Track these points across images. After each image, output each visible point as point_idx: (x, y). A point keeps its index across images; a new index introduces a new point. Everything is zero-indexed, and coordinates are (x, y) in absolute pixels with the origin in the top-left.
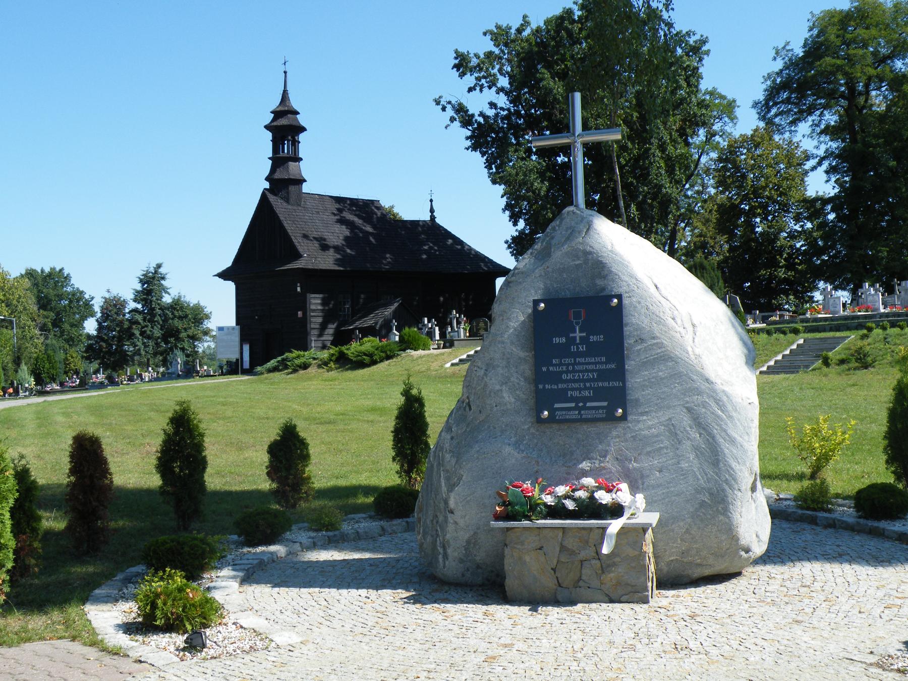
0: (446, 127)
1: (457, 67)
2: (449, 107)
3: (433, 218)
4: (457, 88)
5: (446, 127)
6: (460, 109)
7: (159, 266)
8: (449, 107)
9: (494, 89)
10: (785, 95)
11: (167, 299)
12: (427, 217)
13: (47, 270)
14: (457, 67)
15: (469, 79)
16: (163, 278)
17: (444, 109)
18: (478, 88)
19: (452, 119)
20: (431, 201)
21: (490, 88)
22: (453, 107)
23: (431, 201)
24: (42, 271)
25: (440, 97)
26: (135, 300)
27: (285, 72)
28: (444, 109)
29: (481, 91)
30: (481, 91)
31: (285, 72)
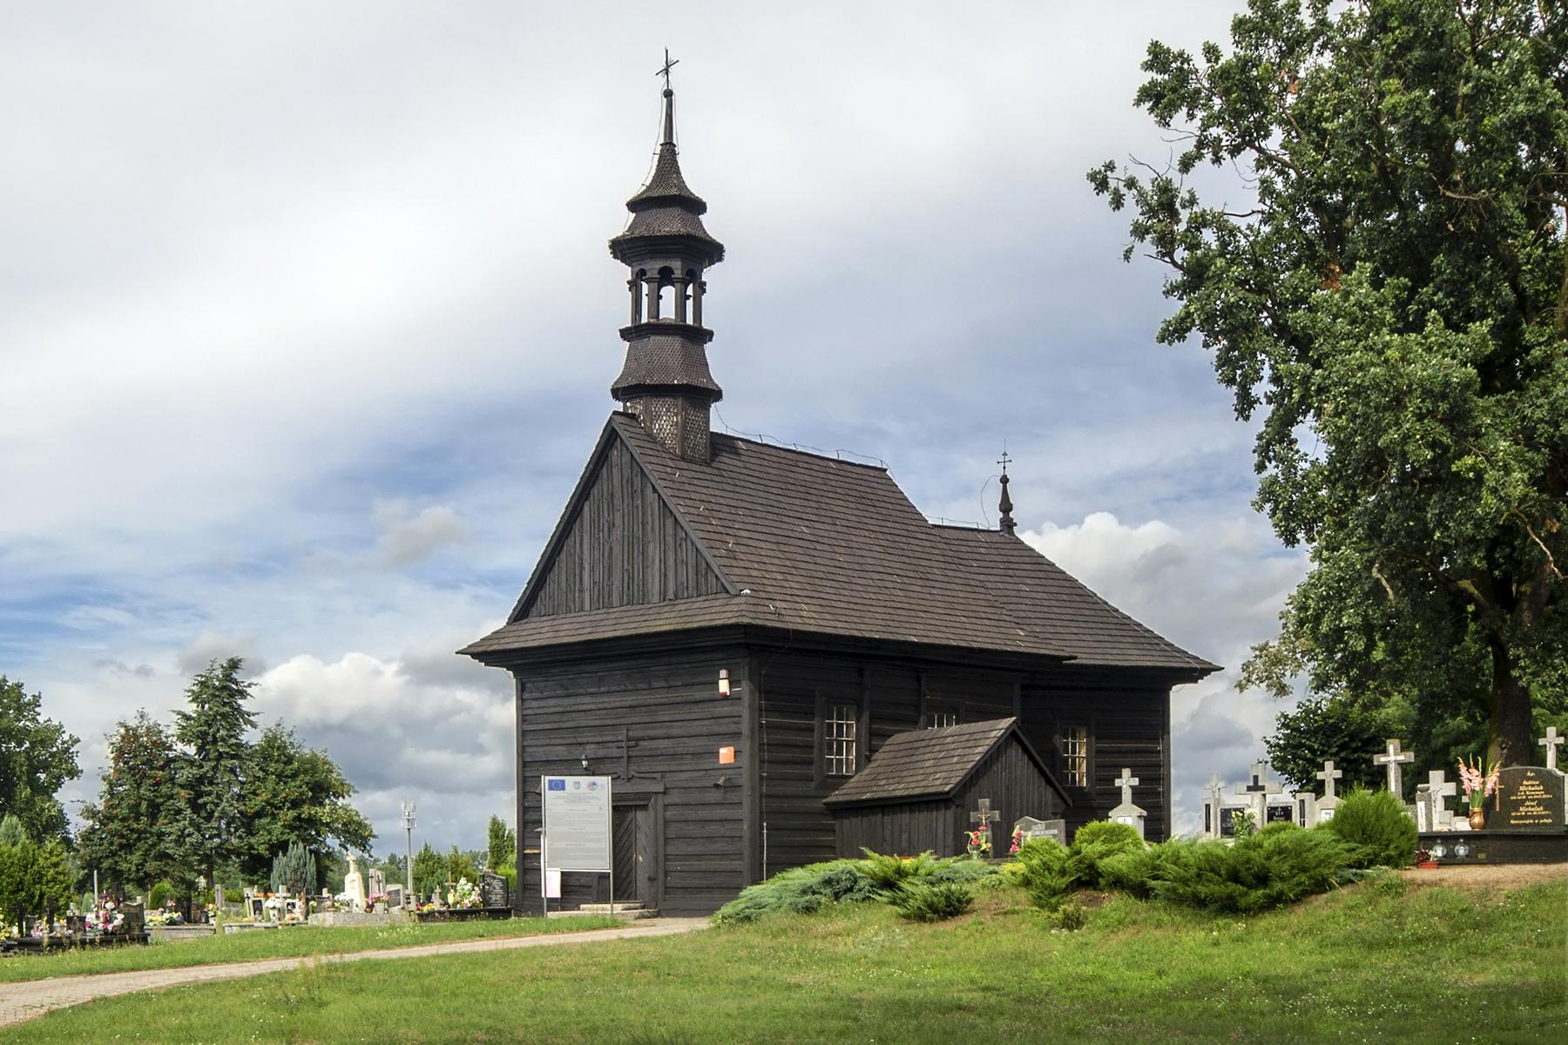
0: (1127, 257)
1: (1149, 94)
2: (1130, 197)
3: (1008, 524)
4: (1154, 147)
5: (1127, 257)
6: (1165, 202)
7: (234, 665)
8: (1130, 197)
11: (251, 737)
12: (993, 522)
15: (1185, 128)
16: (243, 694)
17: (1117, 202)
18: (1208, 155)
19: (1140, 232)
20: (1004, 480)
22: (1142, 198)
23: (1004, 480)
24: (1151, 110)
25: (1110, 167)
27: (668, 94)
28: (1117, 202)
29: (1217, 160)
30: (1217, 160)
31: (668, 94)
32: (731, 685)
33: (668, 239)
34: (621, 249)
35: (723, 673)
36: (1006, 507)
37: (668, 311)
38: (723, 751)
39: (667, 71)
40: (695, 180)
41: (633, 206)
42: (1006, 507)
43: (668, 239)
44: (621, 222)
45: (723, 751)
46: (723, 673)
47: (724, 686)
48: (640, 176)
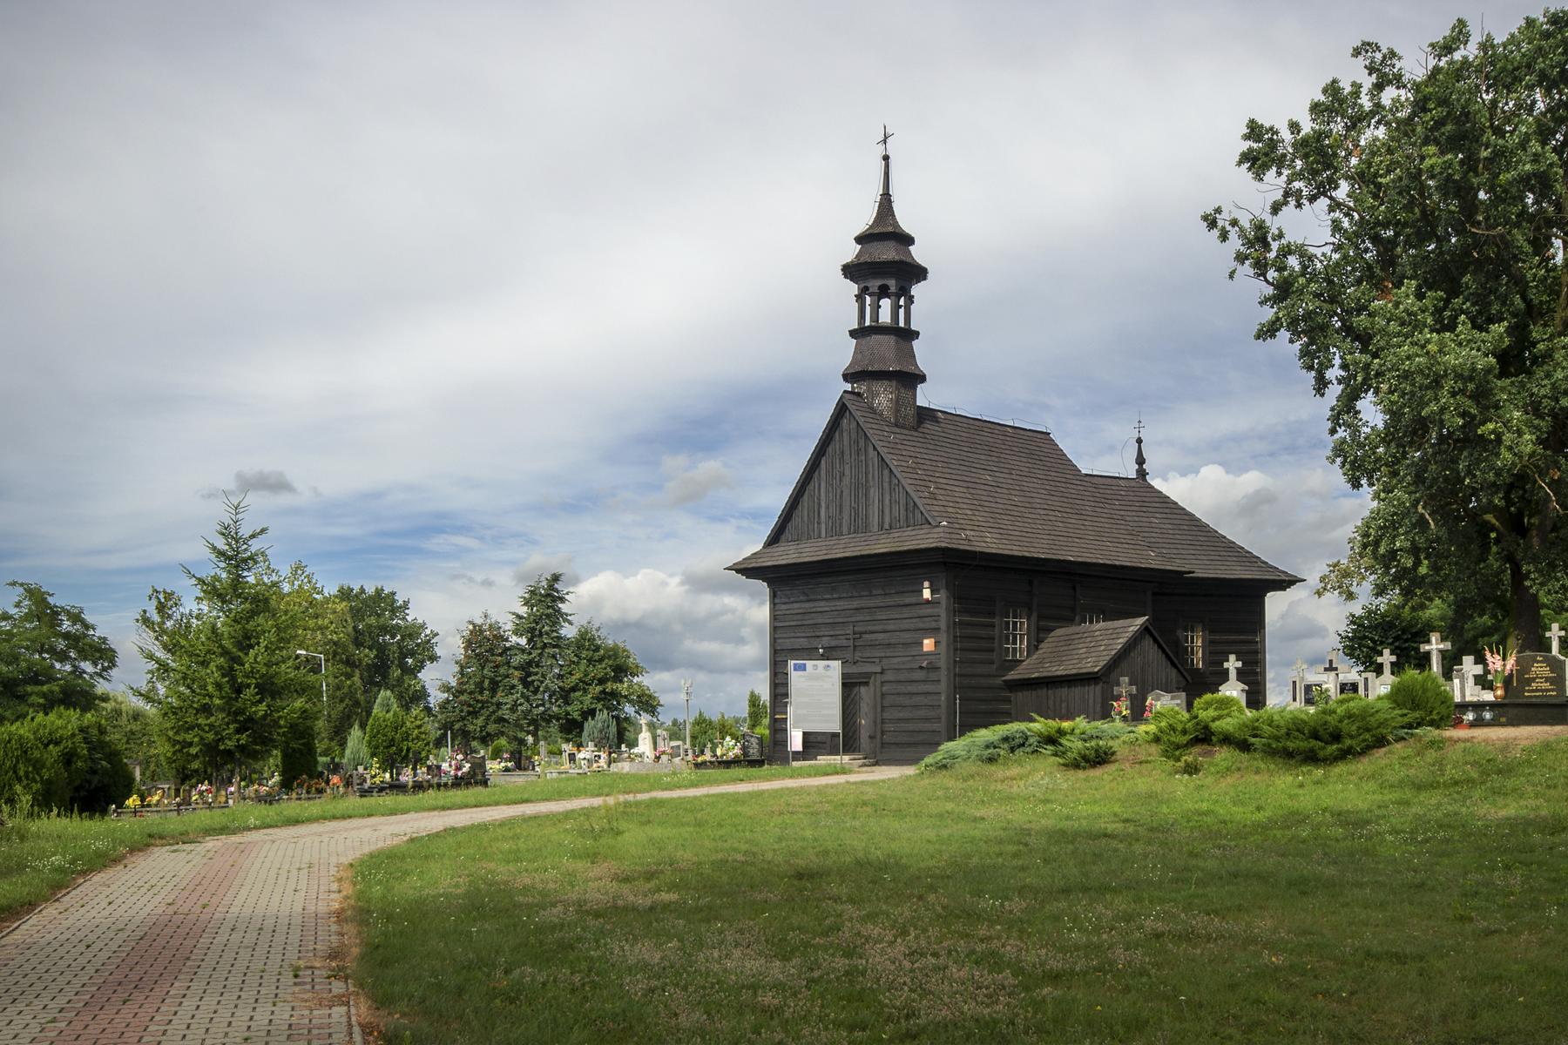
0: (1231, 276)
1: (1248, 158)
2: (1233, 233)
3: (1142, 474)
4: (1252, 197)
7: (556, 578)
8: (1233, 233)
9: (1323, 202)
10: (1359, 379)
11: (568, 632)
12: (1131, 471)
13: (370, 590)
14: (1248, 158)
15: (1274, 182)
16: (562, 600)
17: (1224, 236)
19: (1241, 258)
20: (1139, 441)
21: (1312, 199)
22: (1242, 233)
23: (1139, 441)
25: (1218, 210)
26: (516, 632)
27: (886, 158)
28: (1224, 236)
30: (1299, 206)
31: (886, 158)
32: (932, 593)
33: (885, 263)
34: (850, 271)
35: (926, 584)
36: (1140, 460)
37: (885, 317)
38: (926, 642)
39: (885, 141)
40: (906, 219)
41: (860, 240)
42: (1140, 460)
43: (885, 263)
44: (851, 252)
45: (926, 642)
46: (926, 584)
47: (927, 594)
48: (864, 218)
